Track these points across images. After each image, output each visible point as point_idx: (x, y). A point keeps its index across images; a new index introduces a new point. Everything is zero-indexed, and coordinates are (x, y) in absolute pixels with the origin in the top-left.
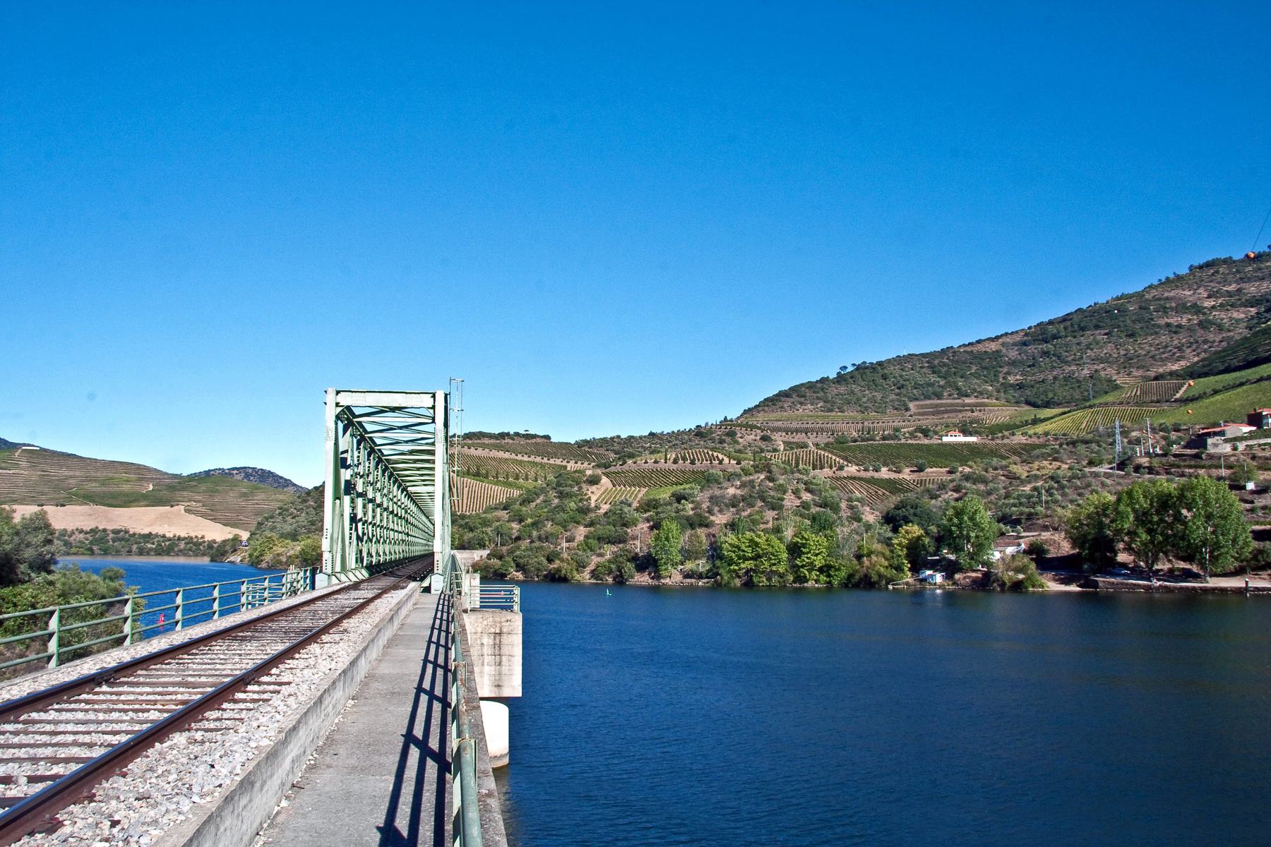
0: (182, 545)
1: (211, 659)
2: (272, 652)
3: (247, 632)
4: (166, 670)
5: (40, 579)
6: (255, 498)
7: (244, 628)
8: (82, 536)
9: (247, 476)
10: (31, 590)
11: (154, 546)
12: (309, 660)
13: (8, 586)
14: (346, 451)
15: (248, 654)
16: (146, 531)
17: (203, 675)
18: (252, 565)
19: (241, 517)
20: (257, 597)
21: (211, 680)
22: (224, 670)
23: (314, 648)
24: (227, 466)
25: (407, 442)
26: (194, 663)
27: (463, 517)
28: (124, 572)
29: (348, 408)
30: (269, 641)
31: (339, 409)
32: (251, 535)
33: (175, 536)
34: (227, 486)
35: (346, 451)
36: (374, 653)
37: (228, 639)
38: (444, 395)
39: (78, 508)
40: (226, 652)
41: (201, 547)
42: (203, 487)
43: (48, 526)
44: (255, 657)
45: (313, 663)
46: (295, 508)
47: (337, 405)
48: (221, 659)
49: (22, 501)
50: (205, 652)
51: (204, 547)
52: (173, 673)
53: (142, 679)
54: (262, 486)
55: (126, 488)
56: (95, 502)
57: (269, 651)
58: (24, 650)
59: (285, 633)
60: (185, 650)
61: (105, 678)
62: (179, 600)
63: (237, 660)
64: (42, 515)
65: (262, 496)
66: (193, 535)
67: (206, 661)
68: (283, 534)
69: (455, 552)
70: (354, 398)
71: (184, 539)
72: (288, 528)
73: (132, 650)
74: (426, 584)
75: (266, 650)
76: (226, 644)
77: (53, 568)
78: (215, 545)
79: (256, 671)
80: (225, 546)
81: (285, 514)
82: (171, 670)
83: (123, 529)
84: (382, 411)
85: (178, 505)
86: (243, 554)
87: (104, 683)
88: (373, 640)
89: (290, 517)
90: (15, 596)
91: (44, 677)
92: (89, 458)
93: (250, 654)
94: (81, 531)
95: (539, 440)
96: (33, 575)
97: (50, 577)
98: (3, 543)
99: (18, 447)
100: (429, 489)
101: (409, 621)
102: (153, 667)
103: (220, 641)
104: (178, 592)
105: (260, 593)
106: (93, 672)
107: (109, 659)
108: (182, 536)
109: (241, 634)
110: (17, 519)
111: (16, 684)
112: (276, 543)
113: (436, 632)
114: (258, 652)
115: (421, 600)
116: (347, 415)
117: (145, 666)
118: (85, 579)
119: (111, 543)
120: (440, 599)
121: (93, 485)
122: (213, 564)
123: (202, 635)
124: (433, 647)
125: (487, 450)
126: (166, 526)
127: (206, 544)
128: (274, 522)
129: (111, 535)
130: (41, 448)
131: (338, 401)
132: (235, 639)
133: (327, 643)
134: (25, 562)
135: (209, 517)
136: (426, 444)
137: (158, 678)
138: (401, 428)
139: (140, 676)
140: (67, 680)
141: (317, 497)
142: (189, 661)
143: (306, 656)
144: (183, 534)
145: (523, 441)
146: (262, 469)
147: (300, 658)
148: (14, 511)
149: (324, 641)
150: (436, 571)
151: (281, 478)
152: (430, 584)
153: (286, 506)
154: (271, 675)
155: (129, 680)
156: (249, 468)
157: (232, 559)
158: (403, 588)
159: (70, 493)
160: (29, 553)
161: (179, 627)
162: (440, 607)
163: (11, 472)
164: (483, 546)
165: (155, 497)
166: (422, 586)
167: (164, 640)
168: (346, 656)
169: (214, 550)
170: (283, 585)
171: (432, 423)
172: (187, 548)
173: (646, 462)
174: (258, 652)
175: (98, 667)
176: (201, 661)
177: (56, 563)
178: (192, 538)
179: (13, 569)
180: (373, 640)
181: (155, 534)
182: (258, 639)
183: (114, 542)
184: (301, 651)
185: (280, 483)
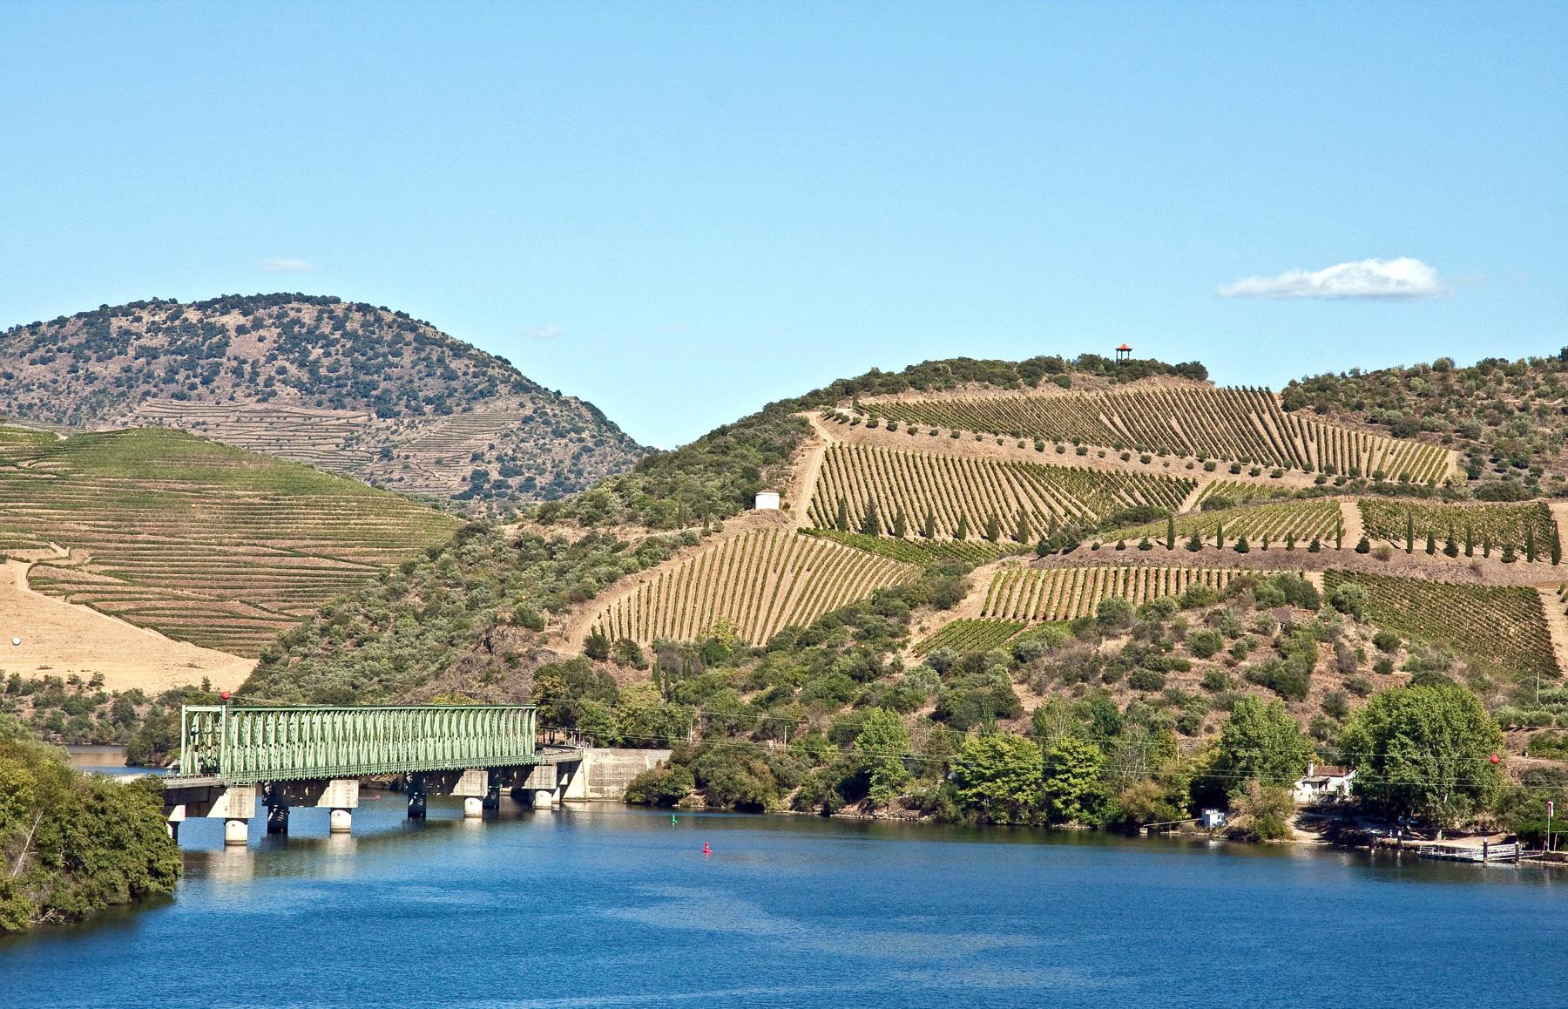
6: (291, 528)
9: (294, 340)
19: (235, 605)
34: (183, 479)
41: (93, 718)
42: (92, 483)
51: (101, 715)
66: (61, 672)
72: (338, 677)
78: (142, 711)
81: (337, 633)
95: (1157, 386)
125: (945, 433)
127: (108, 706)
128: (305, 656)
135: (117, 606)
141: (430, 579)
144: (28, 673)
145: (1095, 392)
146: (364, 308)
151: (460, 350)
153: (345, 606)
156: (301, 298)
164: (662, 745)
172: (43, 723)
173: (1121, 547)
178: (57, 685)
185: (451, 376)
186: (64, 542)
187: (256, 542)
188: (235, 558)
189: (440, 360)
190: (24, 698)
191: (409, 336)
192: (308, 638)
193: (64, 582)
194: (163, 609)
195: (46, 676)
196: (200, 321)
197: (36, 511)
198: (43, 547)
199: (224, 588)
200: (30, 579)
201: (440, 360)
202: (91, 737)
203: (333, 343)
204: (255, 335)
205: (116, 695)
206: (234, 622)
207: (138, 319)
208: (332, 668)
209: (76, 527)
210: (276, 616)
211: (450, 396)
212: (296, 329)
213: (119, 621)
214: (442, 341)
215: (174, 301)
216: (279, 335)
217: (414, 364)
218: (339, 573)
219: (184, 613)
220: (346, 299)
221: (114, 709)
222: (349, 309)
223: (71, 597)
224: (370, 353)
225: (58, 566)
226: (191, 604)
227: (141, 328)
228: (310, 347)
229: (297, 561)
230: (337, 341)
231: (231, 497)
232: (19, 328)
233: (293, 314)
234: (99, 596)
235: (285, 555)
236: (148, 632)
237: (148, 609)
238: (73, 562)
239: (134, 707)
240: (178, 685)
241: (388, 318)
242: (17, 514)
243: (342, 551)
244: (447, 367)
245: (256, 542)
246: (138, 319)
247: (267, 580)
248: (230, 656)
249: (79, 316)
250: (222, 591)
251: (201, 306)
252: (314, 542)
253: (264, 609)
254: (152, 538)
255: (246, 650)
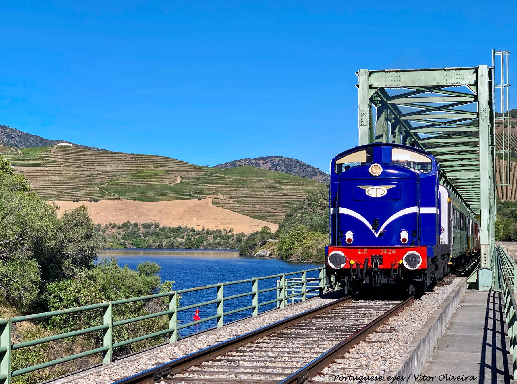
0: (211, 239)
1: (260, 357)
2: (321, 351)
3: (292, 329)
4: (218, 367)
5: (82, 274)
6: (284, 188)
7: (289, 324)
8: (115, 230)
9: (274, 166)
10: (74, 285)
11: (184, 240)
12: (361, 359)
13: (54, 281)
14: (381, 136)
15: (296, 352)
16: (175, 225)
17: (255, 373)
18: (282, 258)
20: (293, 292)
21: (264, 378)
22: (275, 368)
23: (363, 347)
24: (252, 155)
25: (445, 123)
26: (244, 361)
27: (508, 205)
28: (159, 267)
29: (382, 89)
30: (316, 339)
31: (373, 91)
32: (280, 227)
33: (203, 230)
34: (254, 177)
35: (381, 136)
36: (426, 354)
37: (274, 337)
38: (487, 70)
39: (110, 203)
40: (274, 349)
41: (230, 241)
42: (230, 178)
43: (88, 221)
44: (304, 356)
45: (364, 363)
46: (324, 199)
47: (370, 87)
48: (270, 357)
49: (60, 197)
50: (253, 349)
51: (233, 240)
52: (226, 370)
53: (196, 376)
54: (290, 175)
55: (154, 181)
56: (125, 196)
57: (317, 349)
58: (70, 344)
59: (330, 330)
60: (233, 346)
61: (163, 374)
62: (220, 295)
63: (287, 358)
64: (83, 210)
65: (290, 186)
66: (221, 228)
67: (255, 358)
68: (312, 225)
69: (500, 244)
70: (387, 79)
71: (214, 232)
73: (182, 346)
74: (472, 279)
75: (314, 348)
76: (273, 341)
77: (93, 262)
78: (244, 239)
79: (308, 370)
80: (253, 239)
81: (314, 205)
82: (222, 367)
83: (153, 223)
84: (419, 91)
85: (205, 197)
86: (272, 248)
87: (162, 378)
88: (424, 340)
89: (319, 207)
90: (60, 290)
91: (106, 371)
92: (118, 153)
93: (299, 352)
94: (114, 226)
96: (76, 270)
97: (91, 272)
98: (49, 239)
99: (53, 144)
100: (472, 174)
101: (458, 320)
102: (205, 363)
103: (265, 338)
104: (219, 288)
105: (295, 288)
106: (150, 367)
107: (162, 355)
108: (211, 229)
109: (286, 331)
110: (60, 215)
111: (82, 378)
112: (306, 235)
113: (490, 333)
114: (306, 350)
115: (468, 298)
116: (381, 97)
117: (198, 363)
118: (122, 274)
119: (142, 237)
120: (489, 296)
121: (124, 179)
122: (243, 259)
123: (246, 332)
124: (489, 350)
126: (194, 219)
127: (234, 237)
128: (303, 214)
129: (142, 230)
130: (73, 144)
131: (371, 83)
132: (280, 335)
133: (376, 342)
134: (68, 258)
135: (236, 210)
136: (463, 125)
137: (211, 375)
138: (439, 108)
139: (194, 372)
140: (126, 374)
142: (239, 358)
143: (356, 356)
144: (211, 228)
146: (288, 158)
147: (351, 357)
148: (57, 208)
149: (373, 340)
150: (483, 265)
151: (309, 167)
152: (477, 279)
153: (315, 196)
154: (324, 375)
155: (185, 376)
156: (275, 157)
157: (261, 252)
158: (448, 284)
159: (102, 189)
160: (71, 249)
161: (220, 324)
162: (491, 306)
163: (48, 169)
165: (183, 189)
166: (468, 281)
167: (211, 336)
168: (398, 357)
169: (243, 243)
170: (320, 280)
171: (474, 101)
174: (306, 350)
175: (153, 363)
176: (251, 358)
177: (95, 258)
178: (220, 231)
179: (59, 264)
180: (424, 340)
181: (184, 228)
182: (304, 337)
183: (145, 237)
184: (350, 350)
186: (222, 193)
187: (275, 192)
188: (269, 197)
189: (305, 169)
190: (210, 235)
191: (298, 164)
192: (303, 207)
193: (222, 203)
194: (249, 210)
195: (217, 229)
196: (255, 162)
197: (215, 186)
198: (216, 194)
199: (266, 205)
200: (212, 202)
201: (305, 169)
202: (230, 247)
203: (282, 166)
204: (266, 165)
205: (237, 234)
206: (269, 214)
207: (242, 162)
208: (314, 217)
209: (226, 189)
210: (281, 212)
211: (307, 176)
212: (274, 163)
213: (238, 213)
214: (305, 165)
215: (249, 158)
216: (271, 164)
217: (299, 170)
218: (298, 200)
219: (255, 211)
220: (285, 157)
221: (236, 238)
222: (285, 158)
223: (223, 207)
224: (290, 168)
225: (220, 199)
226: (257, 209)
227: (243, 164)
228: (277, 167)
229: (286, 197)
230: (283, 165)
231: (267, 181)
232: (218, 165)
233: (274, 160)
234: (232, 207)
235: (283, 195)
236: (245, 216)
237: (245, 211)
238: (224, 198)
239: (242, 238)
240: (222, 339)
241: (294, 160)
242: (210, 187)
243: (299, 194)
244: (306, 170)
245: (275, 192)
246: (242, 162)
247: (278, 202)
248: (269, 223)
249: (230, 162)
250: (266, 206)
251: (255, 159)
252: (290, 192)
253: (278, 210)
254: (246, 192)
255: (273, 221)
